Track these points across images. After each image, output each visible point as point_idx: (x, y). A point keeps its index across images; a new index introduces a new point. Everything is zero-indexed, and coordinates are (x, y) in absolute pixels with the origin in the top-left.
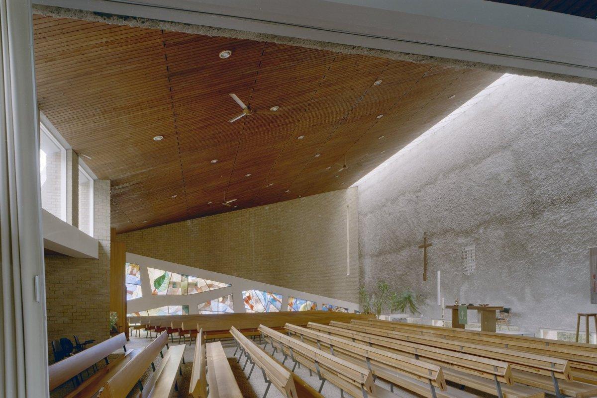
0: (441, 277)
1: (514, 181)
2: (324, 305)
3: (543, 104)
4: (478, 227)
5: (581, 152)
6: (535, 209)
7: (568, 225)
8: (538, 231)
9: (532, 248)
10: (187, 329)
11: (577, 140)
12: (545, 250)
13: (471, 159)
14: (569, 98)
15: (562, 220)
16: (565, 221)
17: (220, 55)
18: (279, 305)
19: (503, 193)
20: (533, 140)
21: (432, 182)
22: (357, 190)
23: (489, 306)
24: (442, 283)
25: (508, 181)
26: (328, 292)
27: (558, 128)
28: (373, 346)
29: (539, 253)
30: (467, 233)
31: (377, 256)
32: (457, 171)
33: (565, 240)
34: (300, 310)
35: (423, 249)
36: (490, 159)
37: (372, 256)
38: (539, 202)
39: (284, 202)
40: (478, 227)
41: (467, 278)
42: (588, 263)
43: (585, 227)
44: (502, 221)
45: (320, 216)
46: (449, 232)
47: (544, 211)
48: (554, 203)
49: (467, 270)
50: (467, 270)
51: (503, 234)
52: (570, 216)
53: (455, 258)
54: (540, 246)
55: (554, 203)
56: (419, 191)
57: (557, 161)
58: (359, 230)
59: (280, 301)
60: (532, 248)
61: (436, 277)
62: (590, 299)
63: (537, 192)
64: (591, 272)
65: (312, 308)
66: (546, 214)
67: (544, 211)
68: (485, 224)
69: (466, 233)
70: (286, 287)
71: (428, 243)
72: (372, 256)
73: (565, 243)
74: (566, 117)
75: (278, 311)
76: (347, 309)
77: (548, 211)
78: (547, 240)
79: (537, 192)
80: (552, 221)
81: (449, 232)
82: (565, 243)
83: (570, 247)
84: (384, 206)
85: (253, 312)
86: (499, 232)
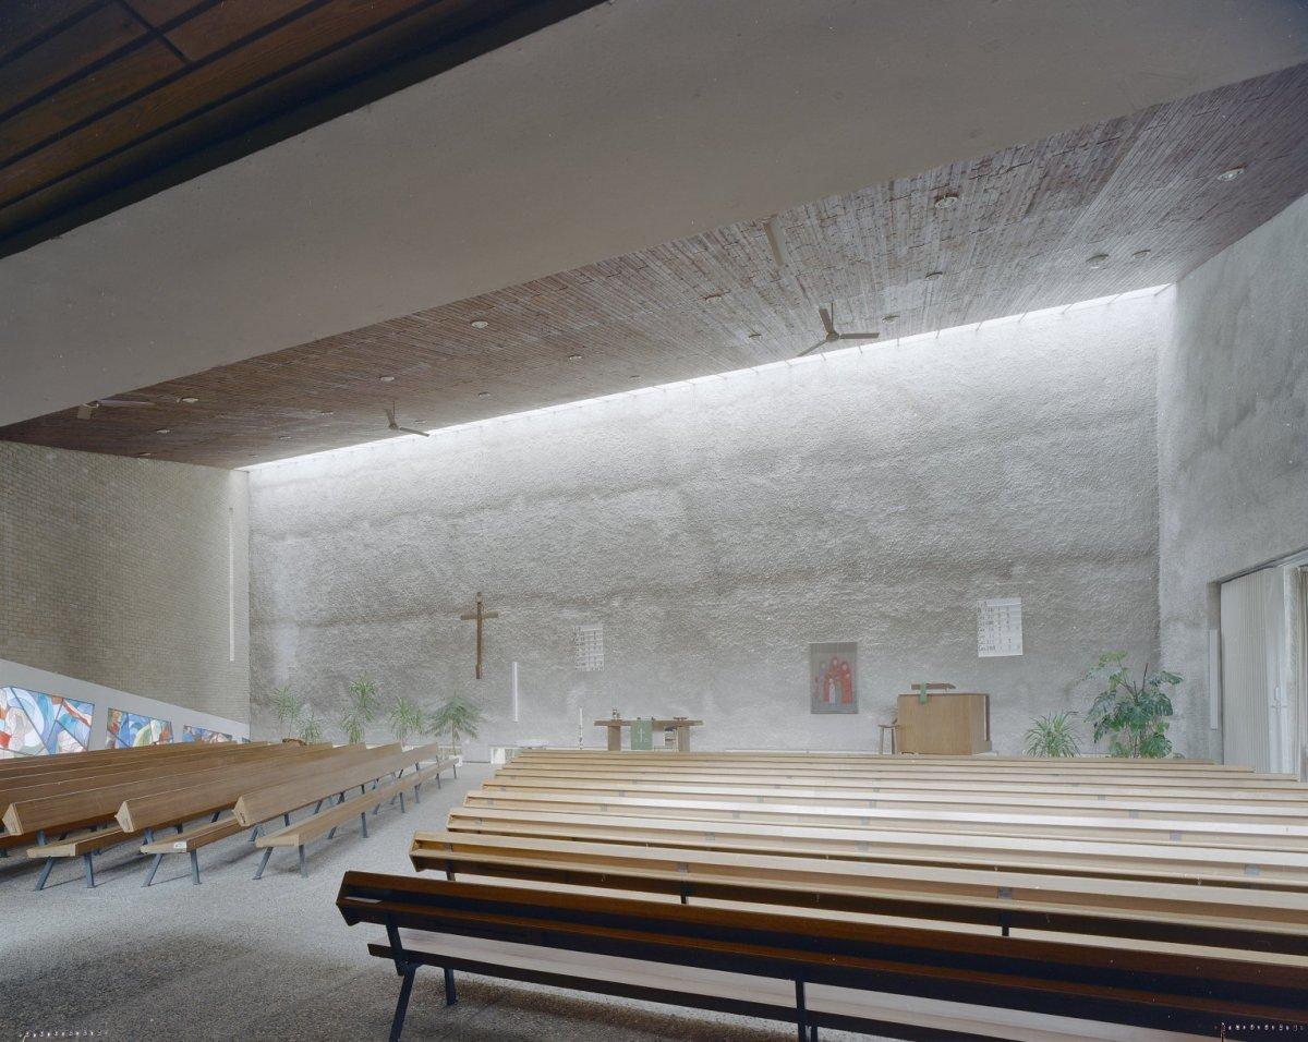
0: (520, 673)
1: (684, 537)
2: (186, 727)
3: (735, 442)
4: (611, 595)
5: (795, 520)
6: (722, 582)
7: (776, 611)
9: (715, 637)
10: (32, 828)
11: (790, 503)
13: (592, 486)
14: (777, 445)
15: (766, 604)
18: (84, 731)
19: (661, 551)
20: (719, 486)
21: (501, 504)
22: (248, 480)
24: (521, 684)
25: (672, 536)
26: (194, 698)
27: (759, 480)
28: (626, 794)
30: (585, 603)
31: (319, 626)
32: (562, 499)
34: (136, 744)
35: (473, 623)
36: (635, 494)
37: (302, 625)
39: (96, 455)
40: (611, 595)
41: (583, 676)
42: (806, 662)
43: (803, 617)
44: (658, 593)
45: (179, 516)
46: (540, 597)
48: (754, 579)
49: (584, 664)
50: (584, 664)
51: (661, 613)
52: (778, 600)
53: (555, 642)
55: (754, 579)
56: (461, 515)
57: (759, 524)
58: (251, 566)
59: (85, 721)
60: (715, 637)
61: (511, 671)
62: (809, 708)
63: (724, 560)
64: (812, 675)
65: (161, 738)
66: (740, 593)
68: (628, 594)
69: (582, 604)
70: (101, 684)
71: (485, 611)
72: (302, 625)
74: (772, 469)
75: (79, 749)
76: (228, 736)
79: (724, 560)
81: (540, 597)
84: (349, 525)
85: (10, 756)
86: (654, 608)
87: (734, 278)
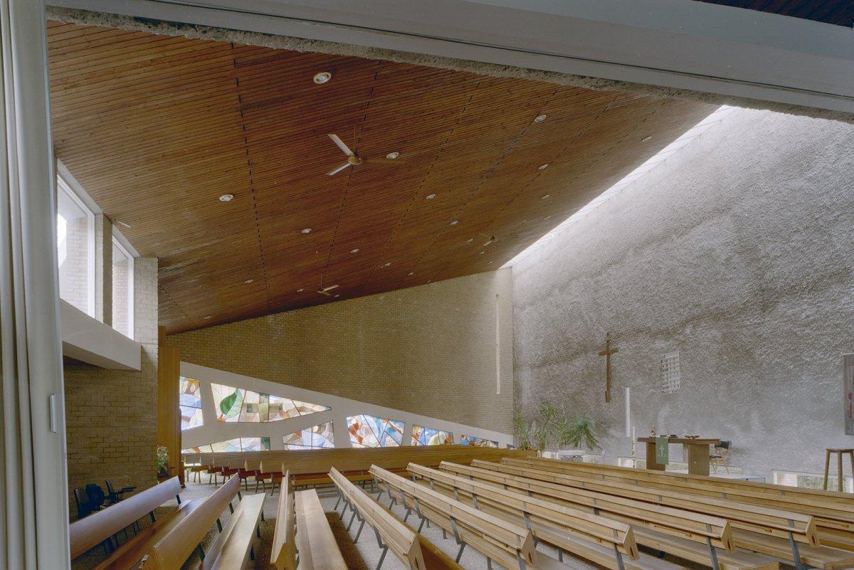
0: (631, 397)
1: (736, 259)
2: (463, 436)
3: (777, 150)
4: (683, 324)
5: (831, 218)
6: (766, 299)
7: (812, 322)
8: (769, 331)
9: (761, 355)
10: (267, 471)
11: (826, 201)
12: (780, 357)
13: (673, 227)
14: (814, 140)
15: (804, 315)
16: (808, 316)
17: (315, 78)
18: (399, 436)
19: (719, 276)
20: (763, 200)
21: (618, 260)
22: (511, 272)
23: (699, 438)
24: (632, 405)
25: (727, 260)
26: (469, 418)
27: (798, 183)
28: (534, 495)
29: (771, 362)
30: (669, 333)
31: (539, 367)
32: (654, 245)
33: (808, 344)
34: (430, 444)
35: (605, 357)
36: (700, 227)
37: (532, 366)
38: (771, 289)
39: (406, 289)
40: (683, 324)
41: (668, 398)
42: (841, 376)
43: (837, 326)
44: (718, 316)
45: (458, 309)
46: (642, 332)
47: (778, 302)
48: (793, 291)
49: (668, 387)
50: (668, 387)
51: (719, 335)
52: (815, 309)
53: (650, 370)
54: (772, 352)
55: (793, 291)
56: (600, 274)
57: (797, 231)
58: (513, 329)
59: (400, 432)
60: (761, 355)
61: (624, 397)
62: (844, 428)
63: (768, 275)
64: (846, 390)
65: (446, 442)
66: (781, 307)
67: (778, 302)
68: (694, 320)
69: (667, 334)
70: (409, 411)
71: (612, 347)
72: (532, 366)
73: (809, 348)
74: (809, 167)
75: (398, 445)
76: (496, 443)
77: (784, 302)
78: (783, 344)
79: (768, 275)
80: (790, 317)
81: (642, 332)
82: (809, 348)
83: (815, 354)
84: (549, 294)
85: (363, 447)
86: (714, 332)
87: (473, 153)
